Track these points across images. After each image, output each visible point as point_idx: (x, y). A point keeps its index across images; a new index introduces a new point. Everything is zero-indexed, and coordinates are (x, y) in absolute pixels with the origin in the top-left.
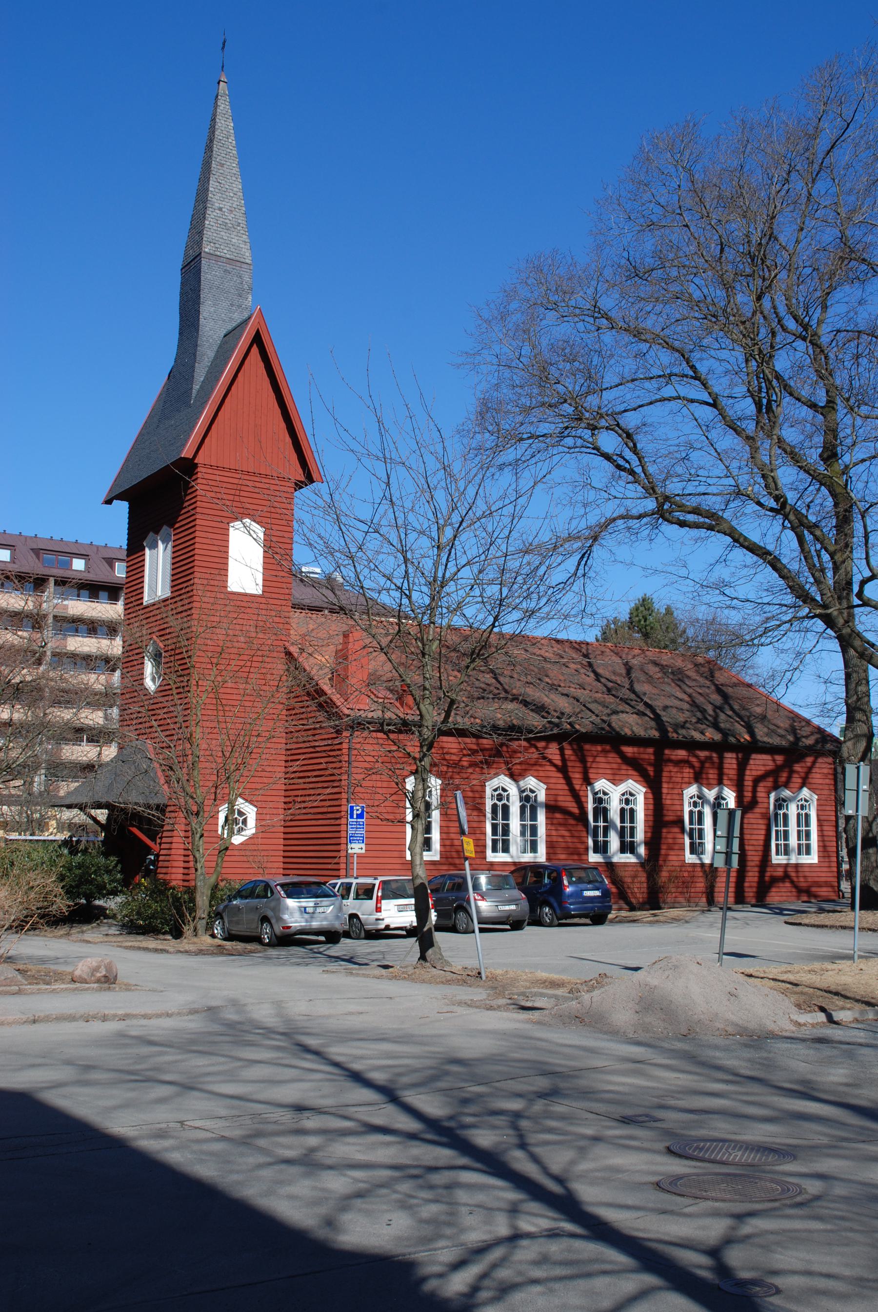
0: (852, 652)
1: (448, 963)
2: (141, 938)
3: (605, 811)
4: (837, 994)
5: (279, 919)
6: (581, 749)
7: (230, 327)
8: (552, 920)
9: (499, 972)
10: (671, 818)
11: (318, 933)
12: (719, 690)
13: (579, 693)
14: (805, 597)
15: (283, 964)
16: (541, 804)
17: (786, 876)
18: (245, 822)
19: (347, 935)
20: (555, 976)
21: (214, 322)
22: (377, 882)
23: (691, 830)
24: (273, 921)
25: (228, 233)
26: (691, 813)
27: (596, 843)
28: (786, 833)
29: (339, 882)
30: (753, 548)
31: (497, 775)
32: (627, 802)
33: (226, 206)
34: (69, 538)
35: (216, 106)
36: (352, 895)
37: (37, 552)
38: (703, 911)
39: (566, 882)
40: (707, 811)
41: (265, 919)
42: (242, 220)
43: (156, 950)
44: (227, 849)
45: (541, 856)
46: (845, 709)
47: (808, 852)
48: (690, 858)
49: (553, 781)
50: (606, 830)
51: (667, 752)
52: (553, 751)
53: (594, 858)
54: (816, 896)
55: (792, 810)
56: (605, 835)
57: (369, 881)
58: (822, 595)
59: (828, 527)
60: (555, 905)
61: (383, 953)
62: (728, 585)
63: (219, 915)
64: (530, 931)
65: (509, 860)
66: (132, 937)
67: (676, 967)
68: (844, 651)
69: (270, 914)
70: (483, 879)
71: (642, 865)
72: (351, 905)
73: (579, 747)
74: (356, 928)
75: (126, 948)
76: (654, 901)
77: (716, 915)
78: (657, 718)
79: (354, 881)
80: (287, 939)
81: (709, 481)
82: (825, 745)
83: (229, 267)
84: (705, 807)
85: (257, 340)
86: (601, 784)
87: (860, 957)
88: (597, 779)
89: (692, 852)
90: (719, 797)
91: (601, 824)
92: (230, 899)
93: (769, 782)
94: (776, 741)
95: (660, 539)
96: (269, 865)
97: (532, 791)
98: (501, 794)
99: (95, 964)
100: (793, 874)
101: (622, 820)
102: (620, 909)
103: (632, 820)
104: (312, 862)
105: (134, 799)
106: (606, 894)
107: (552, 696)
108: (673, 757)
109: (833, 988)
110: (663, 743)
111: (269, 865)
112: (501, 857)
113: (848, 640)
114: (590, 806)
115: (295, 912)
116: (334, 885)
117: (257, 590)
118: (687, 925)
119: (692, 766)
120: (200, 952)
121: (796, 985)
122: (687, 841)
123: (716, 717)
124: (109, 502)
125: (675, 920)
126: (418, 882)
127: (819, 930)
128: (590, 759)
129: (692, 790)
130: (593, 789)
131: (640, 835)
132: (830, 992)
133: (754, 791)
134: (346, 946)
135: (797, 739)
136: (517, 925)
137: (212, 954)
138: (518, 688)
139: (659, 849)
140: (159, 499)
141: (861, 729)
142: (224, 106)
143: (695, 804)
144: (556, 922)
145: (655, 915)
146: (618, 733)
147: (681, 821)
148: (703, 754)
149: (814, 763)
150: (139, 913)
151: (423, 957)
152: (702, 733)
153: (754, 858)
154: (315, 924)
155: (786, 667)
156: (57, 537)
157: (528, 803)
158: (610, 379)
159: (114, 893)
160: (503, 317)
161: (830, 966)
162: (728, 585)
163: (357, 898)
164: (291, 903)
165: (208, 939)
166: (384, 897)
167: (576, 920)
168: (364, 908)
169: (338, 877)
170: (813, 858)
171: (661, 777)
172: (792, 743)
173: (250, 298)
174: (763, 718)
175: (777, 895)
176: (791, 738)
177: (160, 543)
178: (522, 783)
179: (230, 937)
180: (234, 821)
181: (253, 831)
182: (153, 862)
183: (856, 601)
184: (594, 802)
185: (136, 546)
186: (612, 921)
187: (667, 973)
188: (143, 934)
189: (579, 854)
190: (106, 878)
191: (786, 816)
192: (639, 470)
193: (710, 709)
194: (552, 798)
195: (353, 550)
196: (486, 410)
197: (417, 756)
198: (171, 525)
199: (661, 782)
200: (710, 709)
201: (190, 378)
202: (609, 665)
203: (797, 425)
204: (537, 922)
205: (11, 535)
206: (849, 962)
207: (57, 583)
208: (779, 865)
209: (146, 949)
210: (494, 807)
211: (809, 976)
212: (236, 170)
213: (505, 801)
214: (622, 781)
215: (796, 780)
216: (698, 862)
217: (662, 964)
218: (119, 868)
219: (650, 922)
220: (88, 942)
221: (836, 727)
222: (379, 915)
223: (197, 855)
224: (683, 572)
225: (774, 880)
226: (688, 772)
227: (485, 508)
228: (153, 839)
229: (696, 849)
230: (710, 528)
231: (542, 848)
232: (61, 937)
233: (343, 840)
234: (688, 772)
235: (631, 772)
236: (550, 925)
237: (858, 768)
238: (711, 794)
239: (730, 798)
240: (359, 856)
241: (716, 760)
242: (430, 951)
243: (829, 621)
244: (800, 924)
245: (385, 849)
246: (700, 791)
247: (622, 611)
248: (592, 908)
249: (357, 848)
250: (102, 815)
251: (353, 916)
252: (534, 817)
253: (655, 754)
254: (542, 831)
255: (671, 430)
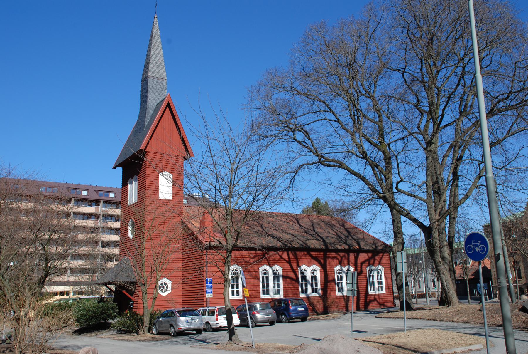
0: (395, 211)
1: (241, 341)
2: (124, 335)
3: (305, 277)
4: (400, 347)
5: (177, 325)
6: (295, 254)
7: (159, 102)
8: (286, 321)
9: (261, 344)
10: (331, 279)
11: (193, 330)
12: (346, 230)
13: (293, 233)
14: (374, 190)
15: (177, 344)
16: (281, 276)
17: (375, 299)
18: (167, 287)
19: (205, 330)
20: (284, 345)
21: (153, 100)
22: (216, 309)
23: (338, 283)
24: (175, 326)
25: (158, 67)
26: (338, 276)
27: (302, 289)
28: (373, 282)
29: (202, 309)
30: (355, 174)
31: (264, 265)
32: (313, 273)
33: (157, 59)
34: (109, 186)
35: (153, 25)
36: (207, 314)
37: (97, 191)
38: (344, 314)
39: (290, 305)
40: (344, 276)
41: (171, 326)
42: (163, 64)
43: (128, 340)
44: (156, 298)
45: (282, 295)
46: (393, 233)
47: (382, 289)
48: (338, 294)
49: (286, 266)
50: (306, 284)
51: (328, 254)
52: (285, 256)
53: (302, 295)
54: (386, 306)
55: (375, 274)
56: (306, 286)
57: (213, 308)
58: (382, 189)
59: (383, 164)
60: (287, 314)
61: (218, 337)
62: (347, 187)
63: (155, 325)
64: (277, 325)
65: (270, 297)
66: (121, 335)
67: (333, 340)
68: (391, 211)
69: (173, 323)
70: (258, 306)
71: (320, 297)
72: (206, 318)
73: (292, 253)
74: (209, 328)
75: (116, 340)
76: (326, 311)
77: (349, 316)
78: (324, 241)
79: (207, 309)
80: (181, 333)
81: (338, 147)
82: (387, 249)
83: (158, 81)
84: (344, 277)
85: (168, 105)
86: (303, 267)
87: (407, 330)
88: (302, 265)
89: (339, 292)
90: (348, 270)
91: (304, 282)
92: (159, 317)
93: (367, 264)
94: (368, 248)
95: (321, 172)
96: (176, 304)
97: (277, 271)
98: (265, 273)
99: (87, 350)
100: (377, 298)
101: (312, 280)
102: (313, 315)
103: (316, 280)
104: (192, 303)
105: (121, 280)
106: (306, 309)
107: (283, 234)
108: (330, 256)
109: (398, 344)
110: (326, 250)
111: (176, 304)
112: (266, 297)
113: (393, 207)
114: (300, 276)
115: (183, 322)
116: (199, 311)
117: (170, 198)
118: (339, 320)
119: (337, 259)
120: (145, 340)
121: (383, 344)
122: (337, 287)
123: (346, 240)
124: (115, 168)
125: (334, 318)
126: (228, 308)
127: (389, 319)
128: (299, 258)
129: (338, 268)
130: (300, 269)
131: (319, 286)
132: (397, 347)
133: (361, 267)
134: (204, 334)
135: (376, 247)
136: (272, 323)
137: (150, 341)
138: (272, 232)
139: (327, 291)
140: (132, 166)
141: (400, 240)
142: (156, 25)
143: (339, 273)
144: (287, 321)
145: (326, 316)
146: (309, 247)
147: (335, 280)
148: (342, 254)
149: (383, 256)
150: (123, 325)
151: (230, 339)
152: (340, 246)
153: (362, 293)
154: (192, 327)
155: (370, 218)
156: (104, 186)
157: (276, 276)
158: (299, 113)
159: (115, 317)
160: (258, 91)
161: (396, 335)
162: (347, 187)
163: (209, 315)
164: (182, 319)
165: (149, 335)
166: (219, 315)
167: (295, 320)
168: (211, 319)
169: (203, 307)
170: (384, 292)
171: (326, 263)
172: (375, 249)
173: (166, 91)
174: (363, 240)
175: (372, 306)
176: (374, 247)
177: (134, 182)
178: (273, 268)
179: (159, 333)
180: (165, 287)
181: (170, 291)
182: (132, 305)
183: (395, 190)
184: (301, 273)
185: (125, 184)
186: (310, 320)
187: (329, 343)
188: (125, 333)
189: (297, 294)
190: (111, 311)
191: (373, 276)
192: (311, 147)
193: (343, 237)
194: (285, 273)
195: (196, 172)
196: (253, 127)
197: (226, 256)
198: (137, 175)
199: (326, 265)
200: (343, 237)
201: (144, 121)
202: (305, 222)
203: (369, 127)
204: (280, 322)
205: (87, 186)
206: (403, 333)
207: (103, 202)
208: (372, 295)
209: (123, 340)
210: (263, 277)
211: (388, 340)
212: (161, 47)
213: (267, 275)
214: (311, 265)
215: (377, 262)
216: (341, 295)
217: (327, 339)
218: (117, 307)
219: (324, 319)
220: (102, 338)
221: (390, 242)
222: (217, 322)
223: (144, 301)
224: (330, 183)
225: (371, 301)
226: (336, 261)
227: (249, 156)
228: (132, 296)
229: (340, 289)
230: (339, 167)
231: (282, 292)
232: (93, 336)
233: (204, 293)
234: (336, 261)
235: (315, 262)
236: (285, 323)
237: (402, 253)
238: (345, 269)
239: (352, 269)
240: (211, 299)
241: (347, 256)
242: (233, 337)
243: (385, 200)
244: (381, 317)
245: (221, 296)
246: (341, 268)
247: (309, 203)
248: (301, 315)
249: (209, 296)
250: (113, 287)
251: (207, 323)
252: (278, 281)
253: (323, 255)
254: (282, 286)
255: (322, 131)
